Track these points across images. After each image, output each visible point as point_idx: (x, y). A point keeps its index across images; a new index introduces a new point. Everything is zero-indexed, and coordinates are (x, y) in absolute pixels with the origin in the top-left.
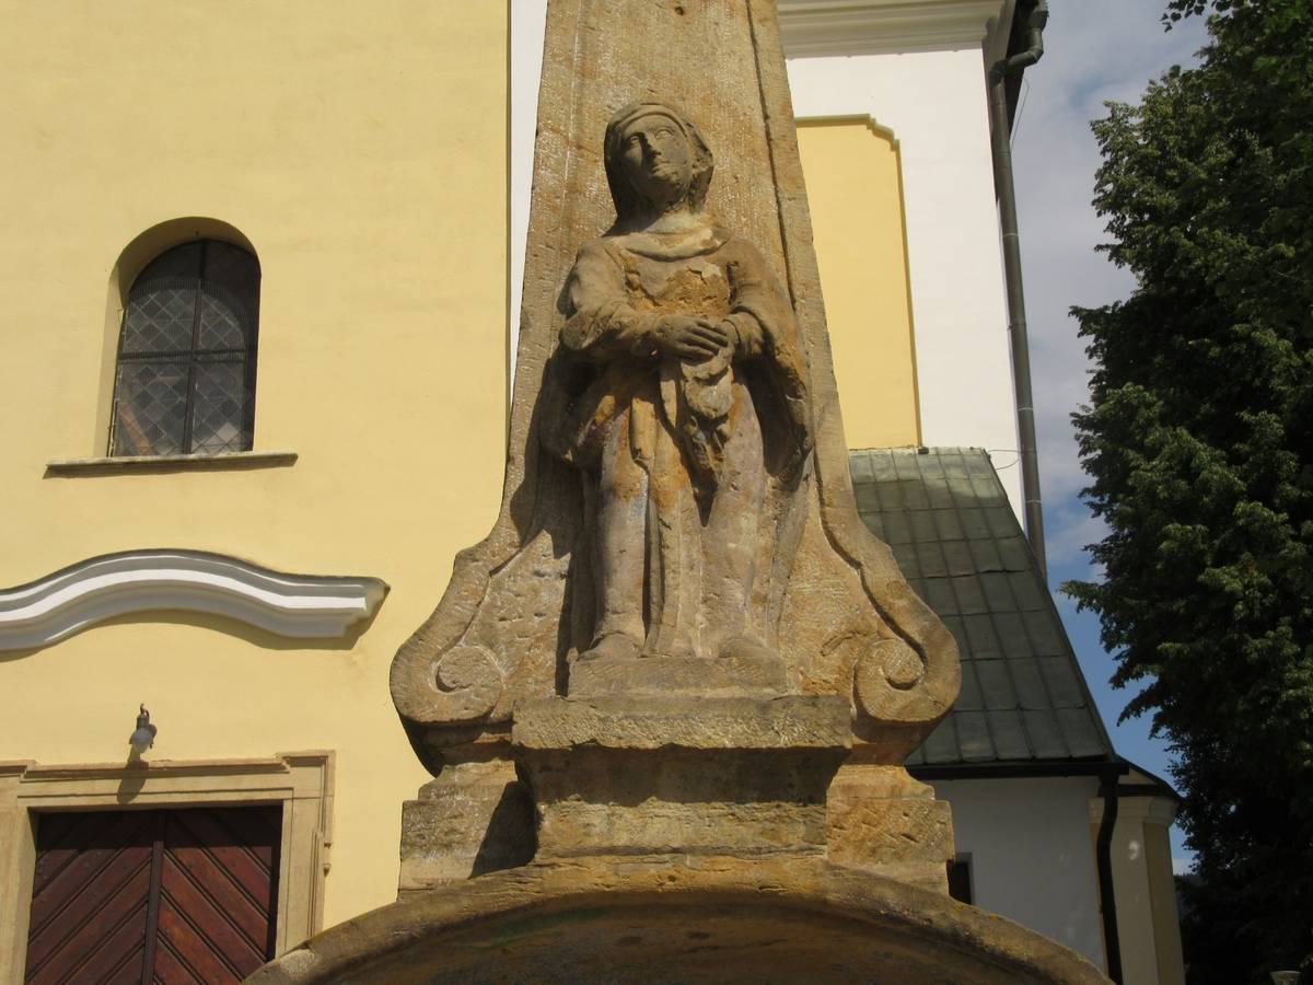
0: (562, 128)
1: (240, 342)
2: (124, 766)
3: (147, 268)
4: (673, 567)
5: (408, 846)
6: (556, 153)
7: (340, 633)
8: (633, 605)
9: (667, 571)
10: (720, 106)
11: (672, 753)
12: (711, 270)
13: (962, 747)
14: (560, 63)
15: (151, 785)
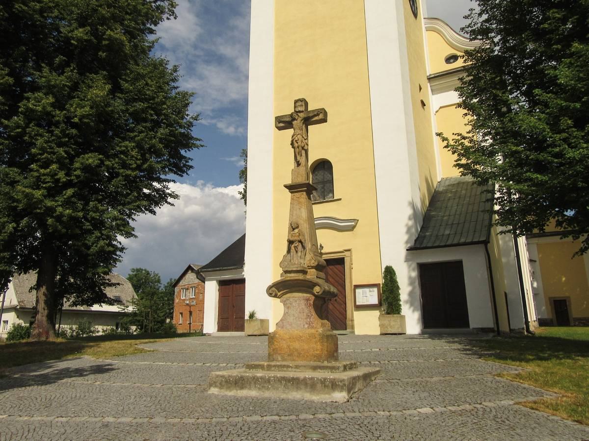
1: (331, 179)
3: (316, 167)
5: (281, 276)
7: (351, 228)
11: (292, 271)
12: (298, 234)
15: (323, 256)
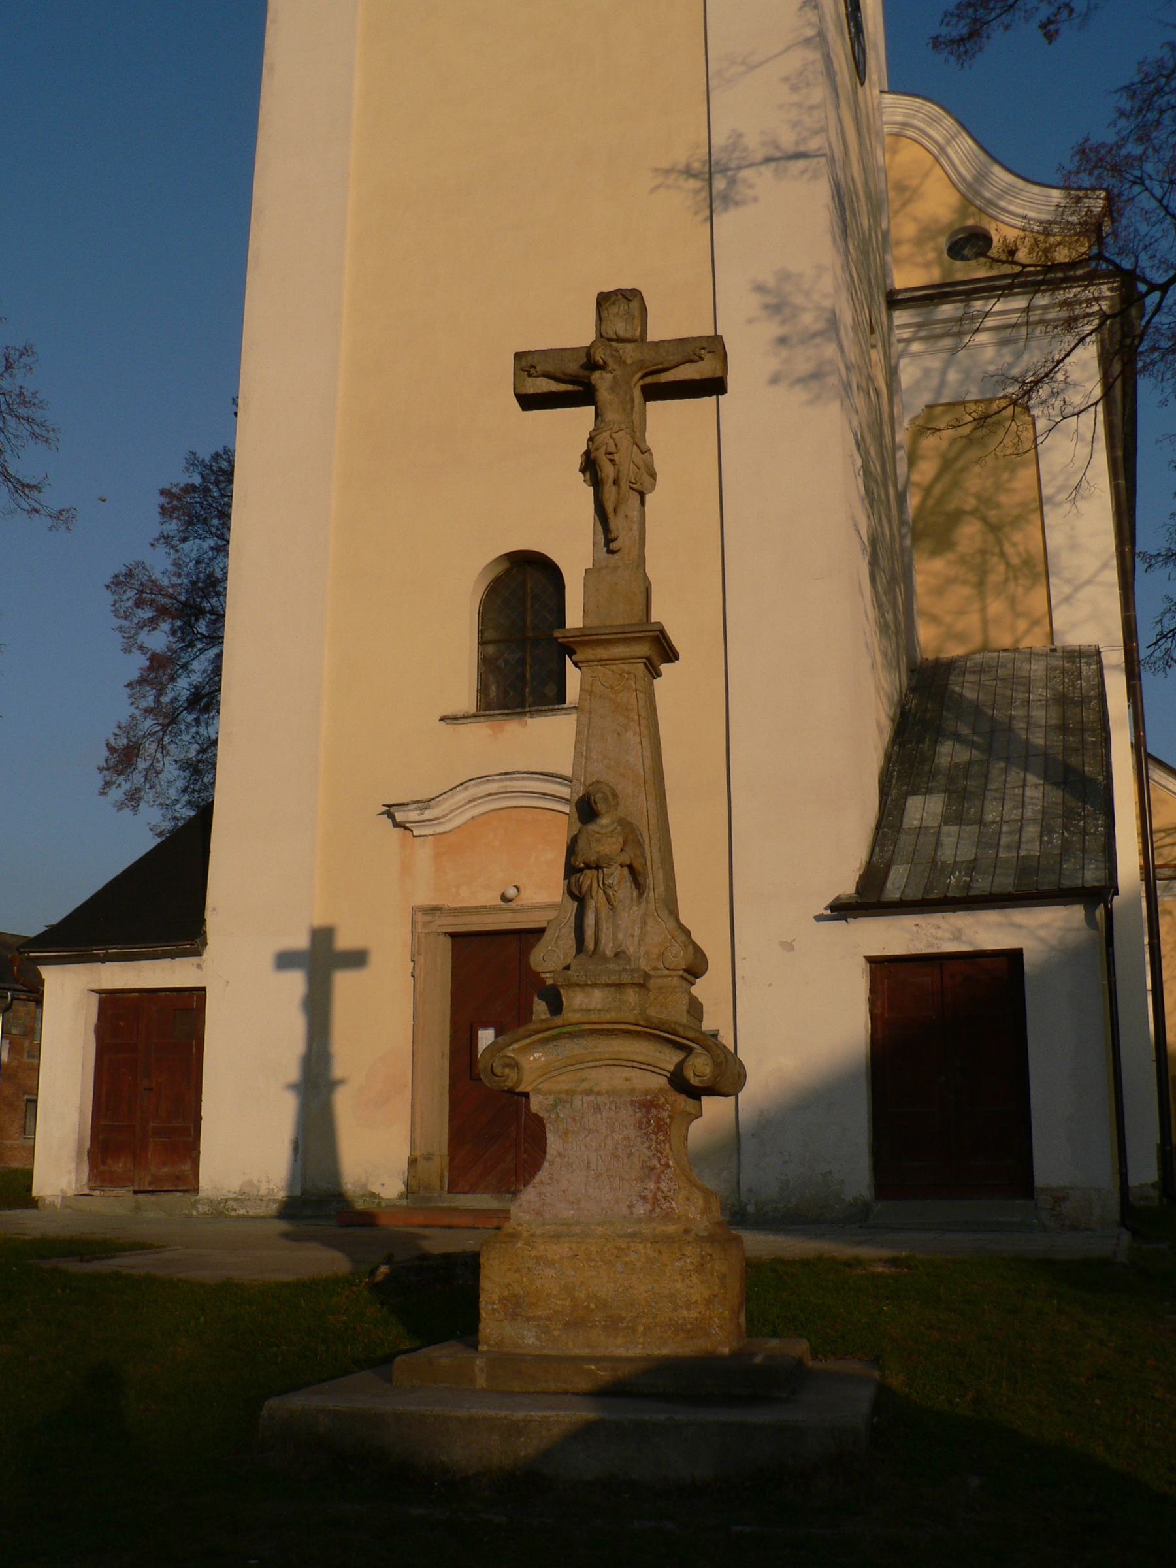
13: (577, 1007)
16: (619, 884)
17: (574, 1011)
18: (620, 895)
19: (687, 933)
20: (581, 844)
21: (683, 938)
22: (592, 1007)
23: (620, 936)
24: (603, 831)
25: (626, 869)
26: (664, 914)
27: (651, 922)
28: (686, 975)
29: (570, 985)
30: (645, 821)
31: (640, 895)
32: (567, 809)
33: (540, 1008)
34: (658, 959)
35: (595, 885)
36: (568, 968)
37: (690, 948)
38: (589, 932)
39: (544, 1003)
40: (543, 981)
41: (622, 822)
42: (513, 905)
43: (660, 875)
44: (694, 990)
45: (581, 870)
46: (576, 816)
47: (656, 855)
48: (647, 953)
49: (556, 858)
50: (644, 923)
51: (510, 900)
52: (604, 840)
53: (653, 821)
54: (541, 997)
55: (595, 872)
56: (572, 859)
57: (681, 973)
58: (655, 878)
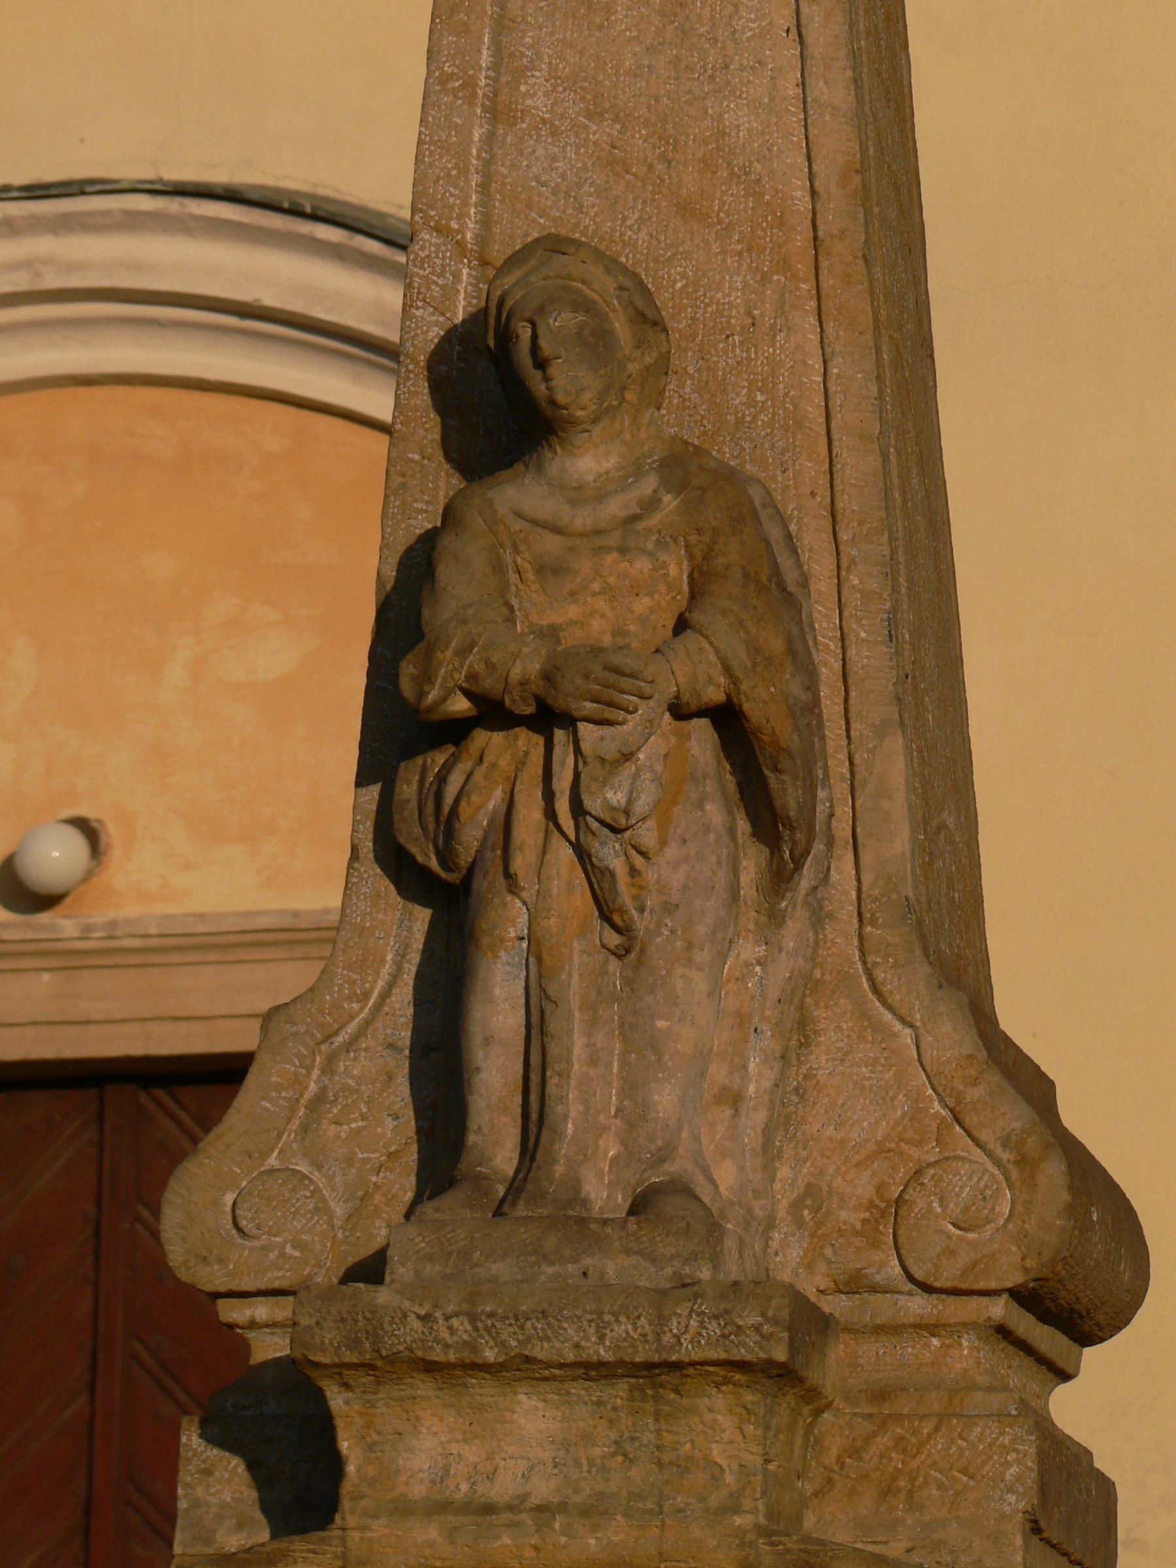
0: (454, 225)
2: (426, 613)
4: (557, 1067)
6: (441, 275)
8: (505, 1119)
9: (548, 1073)
10: (732, 174)
13: (418, 1491)
14: (454, 92)
16: (663, 812)
17: (403, 1509)
18: (669, 871)
19: (1035, 1088)
20: (459, 583)
21: (1014, 1116)
22: (502, 1489)
23: (665, 1099)
24: (582, 519)
25: (702, 727)
26: (911, 983)
27: (834, 1025)
28: (1026, 1325)
29: (386, 1367)
30: (812, 469)
31: (779, 878)
32: (376, 398)
33: (215, 1490)
34: (869, 1233)
35: (529, 814)
36: (371, 1270)
37: (1053, 1171)
38: (494, 1075)
39: (236, 1464)
40: (232, 1341)
41: (685, 468)
42: (61, 925)
43: (892, 765)
44: (1068, 1408)
45: (454, 732)
46: (428, 428)
47: (872, 658)
48: (812, 1197)
49: (308, 675)
50: (801, 1032)
51: (46, 901)
52: (581, 547)
53: (859, 466)
54: (220, 1432)
55: (528, 741)
56: (408, 670)
57: (998, 1309)
58: (862, 784)
